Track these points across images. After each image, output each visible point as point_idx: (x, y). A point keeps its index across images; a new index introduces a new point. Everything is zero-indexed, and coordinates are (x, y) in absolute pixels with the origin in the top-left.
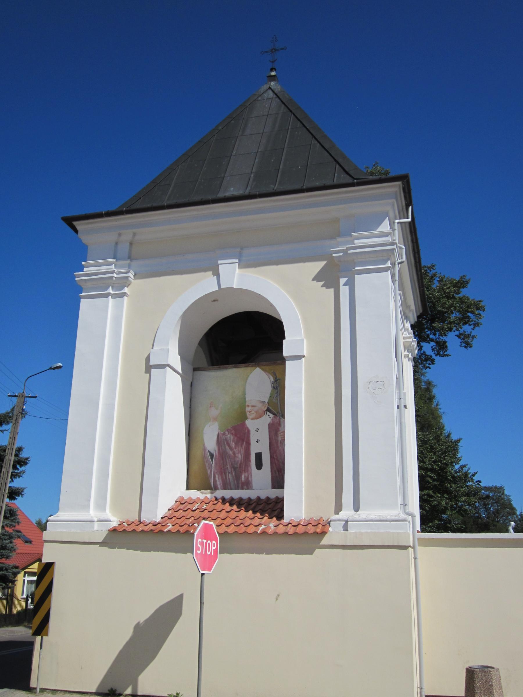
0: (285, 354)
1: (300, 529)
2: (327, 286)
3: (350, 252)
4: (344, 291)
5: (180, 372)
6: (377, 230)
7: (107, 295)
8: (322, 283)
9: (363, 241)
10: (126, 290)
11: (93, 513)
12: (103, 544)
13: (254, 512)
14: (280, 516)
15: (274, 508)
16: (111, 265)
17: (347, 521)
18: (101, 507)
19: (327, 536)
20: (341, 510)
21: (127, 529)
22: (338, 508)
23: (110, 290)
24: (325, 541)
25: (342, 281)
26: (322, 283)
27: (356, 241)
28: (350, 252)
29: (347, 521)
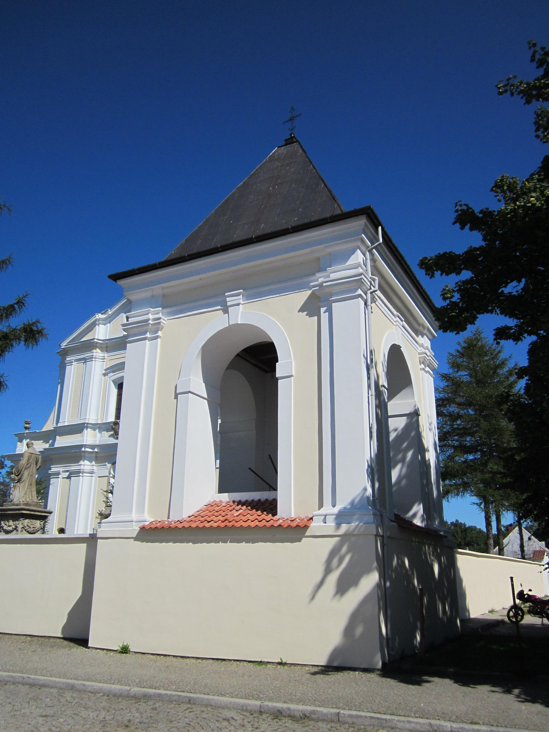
0: (278, 375)
1: (187, 525)
2: (310, 315)
3: (324, 284)
4: (325, 317)
5: (206, 397)
6: (347, 264)
7: (145, 339)
8: (306, 313)
9: (337, 273)
10: (160, 333)
11: (134, 516)
12: (136, 539)
13: (262, 512)
14: (275, 514)
15: (270, 507)
16: (158, 314)
17: (326, 516)
18: (141, 509)
19: (309, 530)
20: (322, 506)
21: (300, 525)
22: (321, 506)
23: (148, 335)
24: (307, 534)
25: (323, 310)
26: (306, 313)
27: (332, 275)
28: (324, 284)
29: (326, 516)
